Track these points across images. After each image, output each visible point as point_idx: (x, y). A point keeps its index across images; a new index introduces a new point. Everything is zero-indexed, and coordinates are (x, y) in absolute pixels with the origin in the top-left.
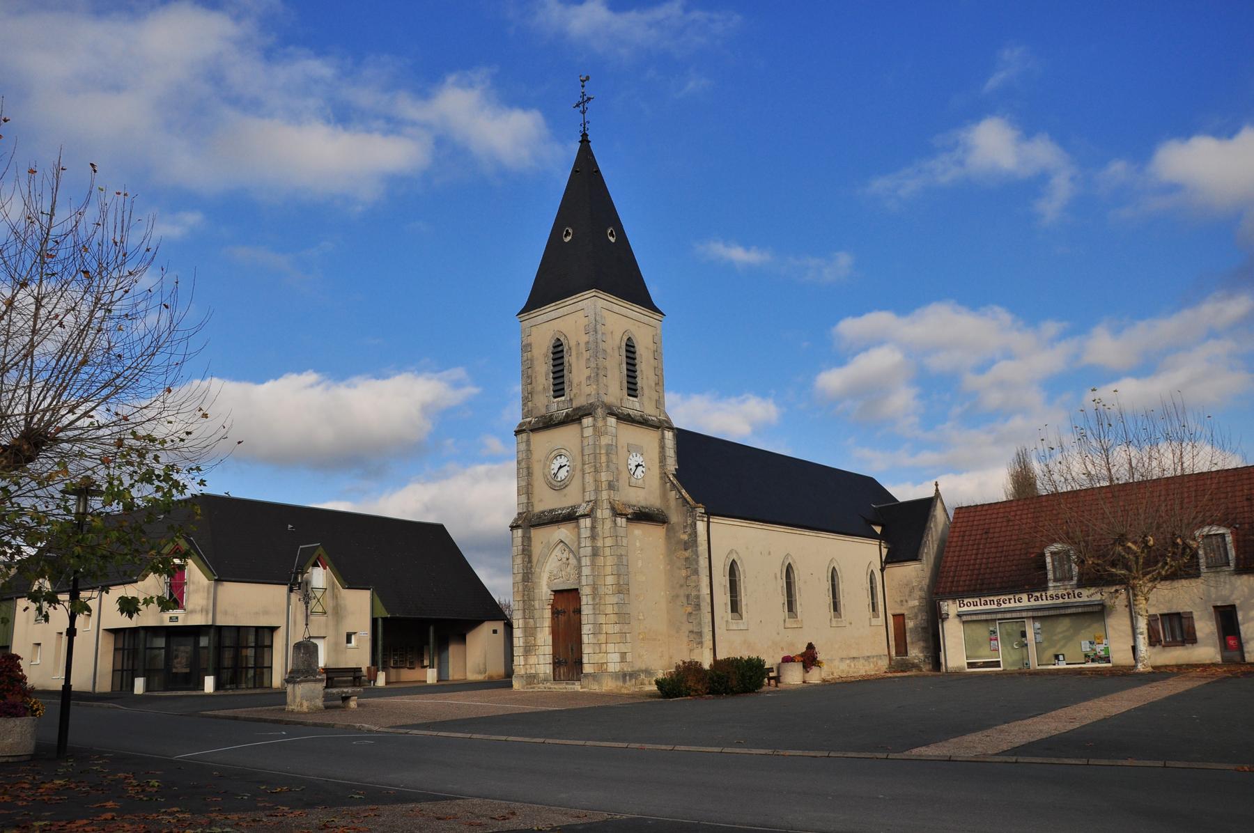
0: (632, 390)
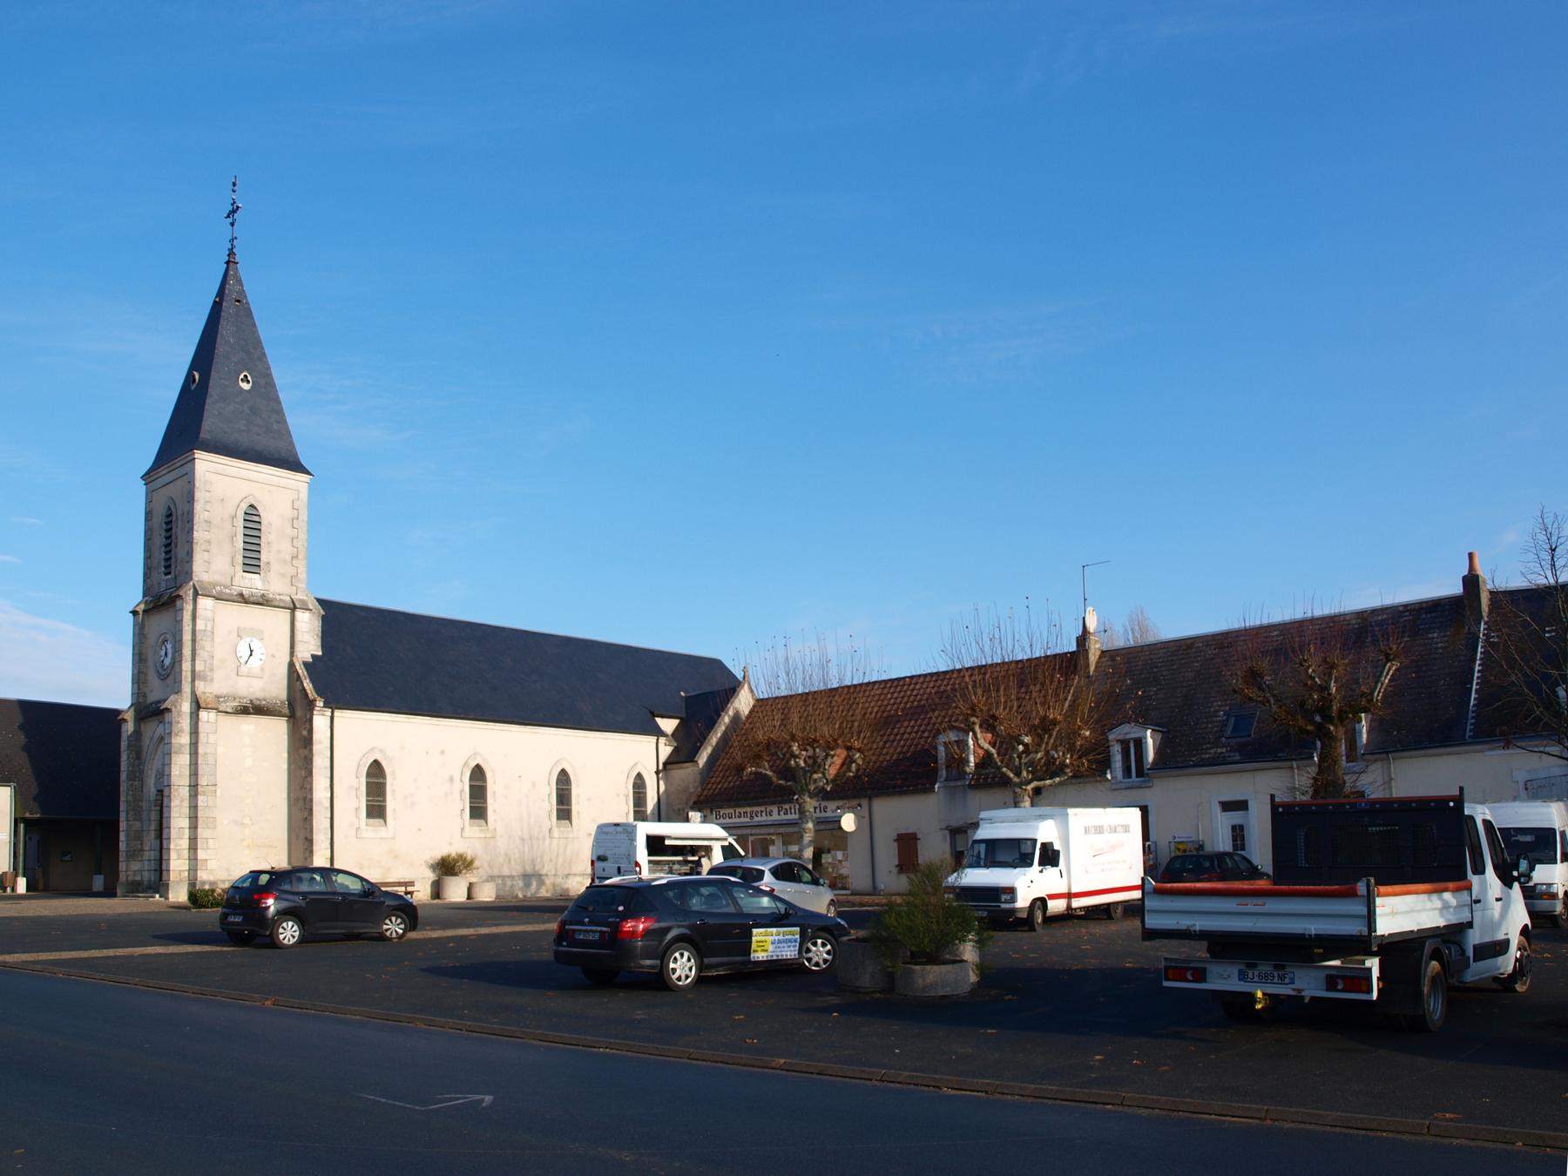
0: (252, 563)
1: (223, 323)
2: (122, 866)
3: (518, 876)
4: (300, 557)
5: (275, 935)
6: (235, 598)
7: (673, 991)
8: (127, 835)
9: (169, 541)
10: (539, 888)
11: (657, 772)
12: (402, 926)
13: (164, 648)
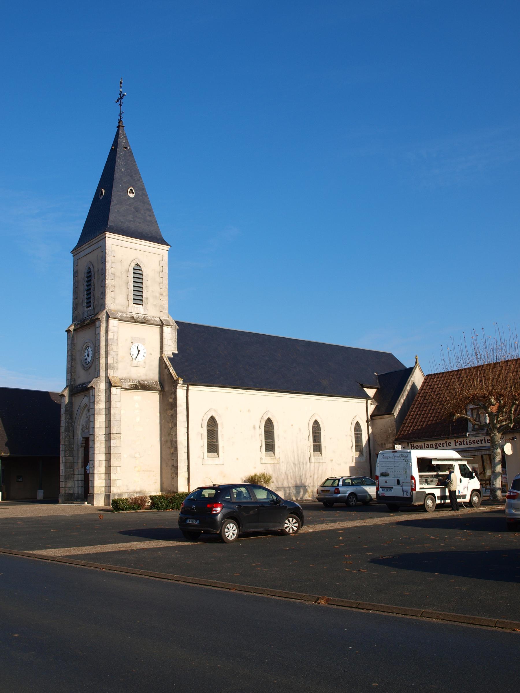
0: (138, 299)
1: (118, 160)
2: (62, 485)
3: (293, 487)
4: (164, 294)
5: (223, 533)
6: (129, 319)
7: (226, 543)
8: (65, 465)
9: (89, 287)
10: (304, 495)
11: (367, 421)
12: (297, 525)
13: (86, 351)
